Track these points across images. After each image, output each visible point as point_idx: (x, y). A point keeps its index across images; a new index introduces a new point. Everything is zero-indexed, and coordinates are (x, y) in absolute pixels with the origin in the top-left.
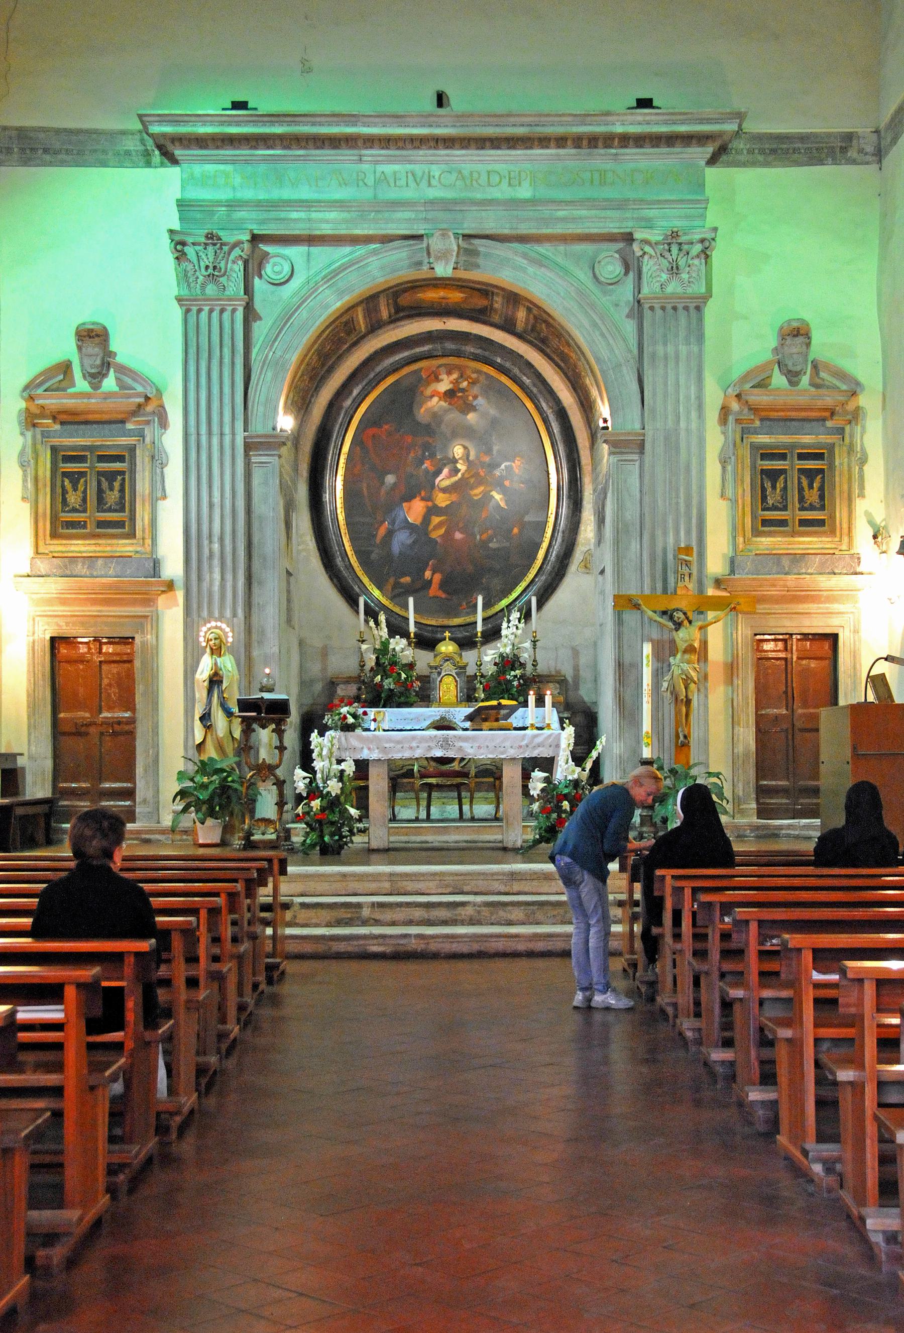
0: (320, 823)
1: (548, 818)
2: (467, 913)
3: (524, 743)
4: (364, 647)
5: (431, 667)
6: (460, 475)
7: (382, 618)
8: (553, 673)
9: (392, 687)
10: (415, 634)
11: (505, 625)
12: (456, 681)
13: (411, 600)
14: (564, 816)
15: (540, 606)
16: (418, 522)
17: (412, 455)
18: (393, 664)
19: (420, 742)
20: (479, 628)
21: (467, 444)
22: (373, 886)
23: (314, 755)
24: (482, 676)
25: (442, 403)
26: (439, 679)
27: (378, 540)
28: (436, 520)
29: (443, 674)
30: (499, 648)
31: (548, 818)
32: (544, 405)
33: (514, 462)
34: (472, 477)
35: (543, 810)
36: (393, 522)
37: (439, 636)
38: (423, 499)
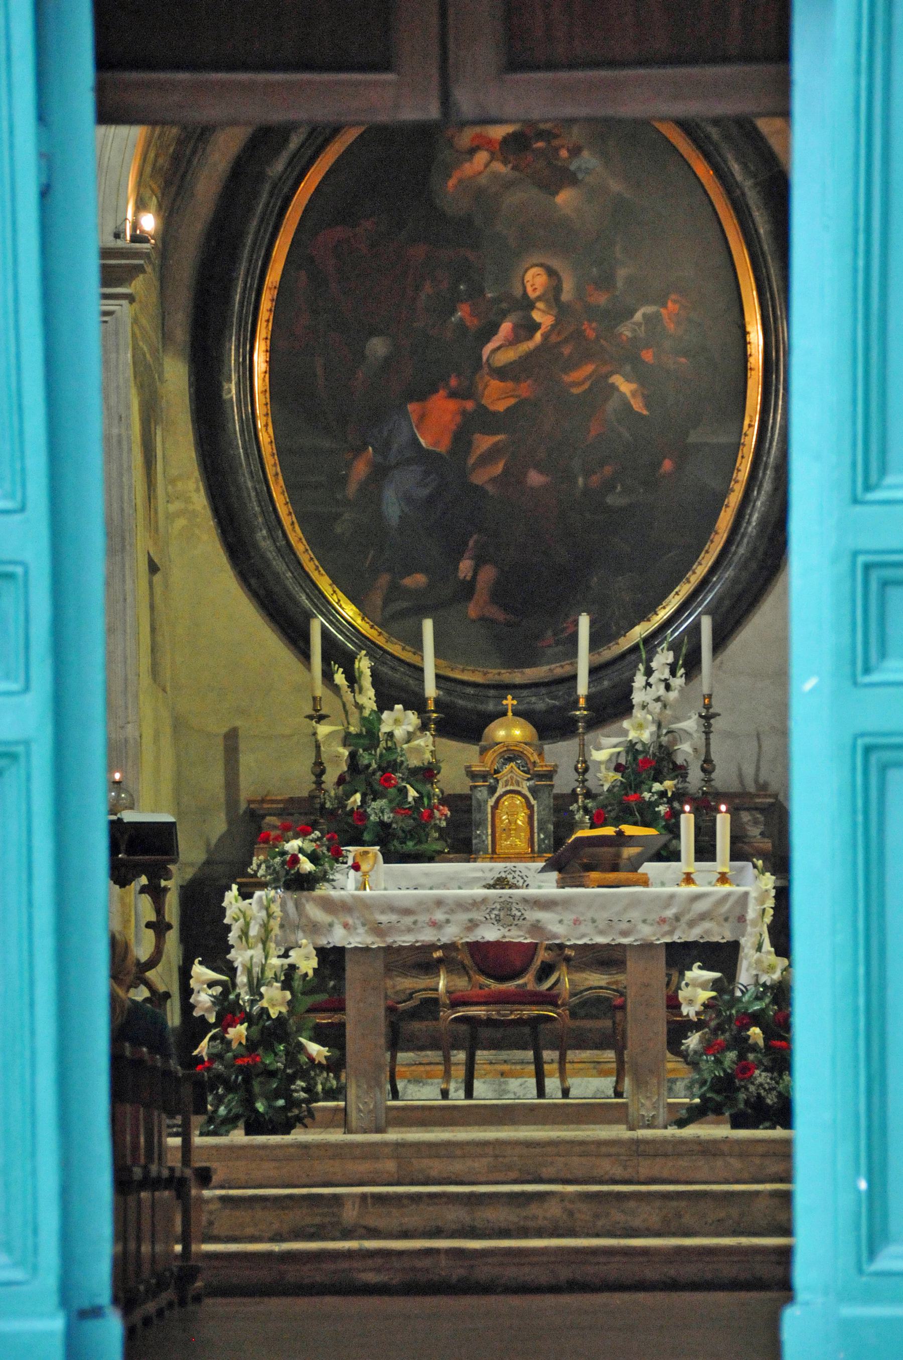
0: (248, 1074)
1: (718, 1062)
2: (548, 1215)
3: (670, 913)
4: (323, 730)
5: (473, 775)
6: (538, 336)
7: (364, 665)
8: (752, 789)
9: (387, 817)
10: (437, 701)
11: (639, 680)
12: (530, 807)
13: (428, 626)
14: (751, 1056)
15: (720, 641)
16: (442, 449)
17: (428, 288)
18: (390, 766)
19: (452, 911)
20: (583, 688)
21: (555, 263)
22: (363, 1168)
23: (232, 937)
24: (588, 795)
25: (498, 167)
26: (491, 802)
27: (352, 489)
28: (484, 443)
29: (500, 790)
30: (625, 733)
31: (718, 1062)
32: (736, 168)
33: (664, 305)
34: (566, 340)
35: (708, 1047)
36: (384, 448)
37: (491, 707)
38: (453, 395)
